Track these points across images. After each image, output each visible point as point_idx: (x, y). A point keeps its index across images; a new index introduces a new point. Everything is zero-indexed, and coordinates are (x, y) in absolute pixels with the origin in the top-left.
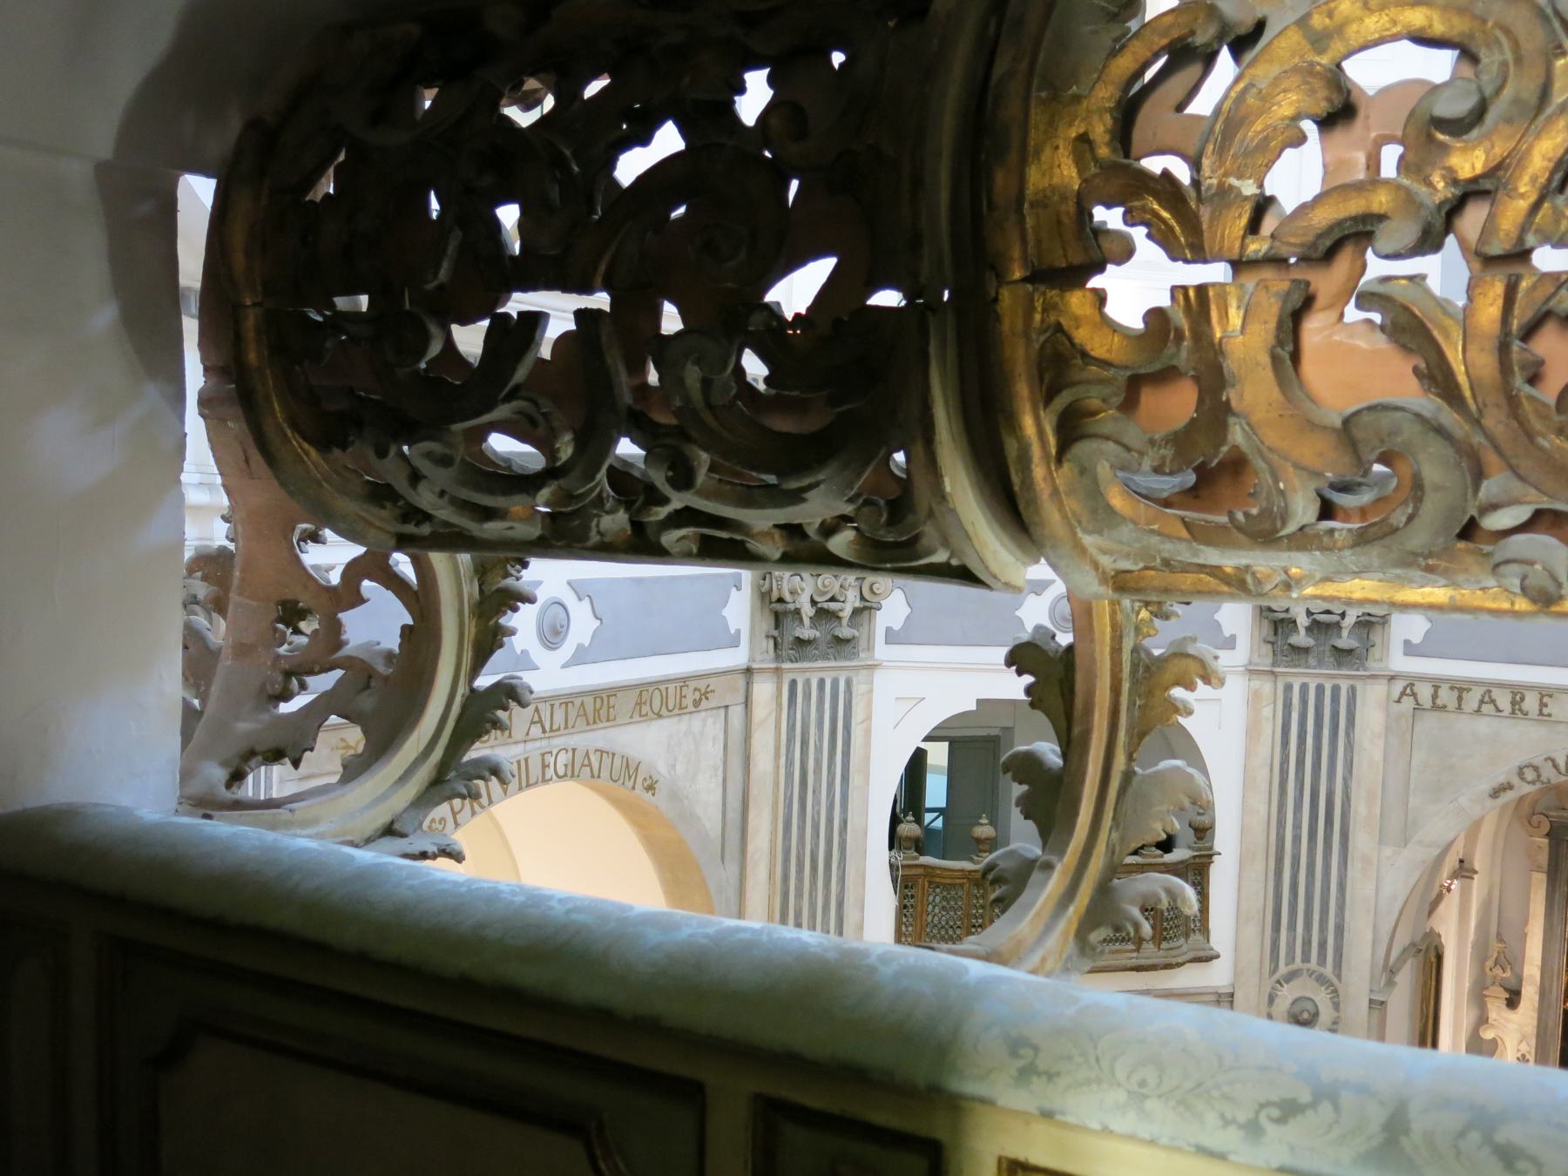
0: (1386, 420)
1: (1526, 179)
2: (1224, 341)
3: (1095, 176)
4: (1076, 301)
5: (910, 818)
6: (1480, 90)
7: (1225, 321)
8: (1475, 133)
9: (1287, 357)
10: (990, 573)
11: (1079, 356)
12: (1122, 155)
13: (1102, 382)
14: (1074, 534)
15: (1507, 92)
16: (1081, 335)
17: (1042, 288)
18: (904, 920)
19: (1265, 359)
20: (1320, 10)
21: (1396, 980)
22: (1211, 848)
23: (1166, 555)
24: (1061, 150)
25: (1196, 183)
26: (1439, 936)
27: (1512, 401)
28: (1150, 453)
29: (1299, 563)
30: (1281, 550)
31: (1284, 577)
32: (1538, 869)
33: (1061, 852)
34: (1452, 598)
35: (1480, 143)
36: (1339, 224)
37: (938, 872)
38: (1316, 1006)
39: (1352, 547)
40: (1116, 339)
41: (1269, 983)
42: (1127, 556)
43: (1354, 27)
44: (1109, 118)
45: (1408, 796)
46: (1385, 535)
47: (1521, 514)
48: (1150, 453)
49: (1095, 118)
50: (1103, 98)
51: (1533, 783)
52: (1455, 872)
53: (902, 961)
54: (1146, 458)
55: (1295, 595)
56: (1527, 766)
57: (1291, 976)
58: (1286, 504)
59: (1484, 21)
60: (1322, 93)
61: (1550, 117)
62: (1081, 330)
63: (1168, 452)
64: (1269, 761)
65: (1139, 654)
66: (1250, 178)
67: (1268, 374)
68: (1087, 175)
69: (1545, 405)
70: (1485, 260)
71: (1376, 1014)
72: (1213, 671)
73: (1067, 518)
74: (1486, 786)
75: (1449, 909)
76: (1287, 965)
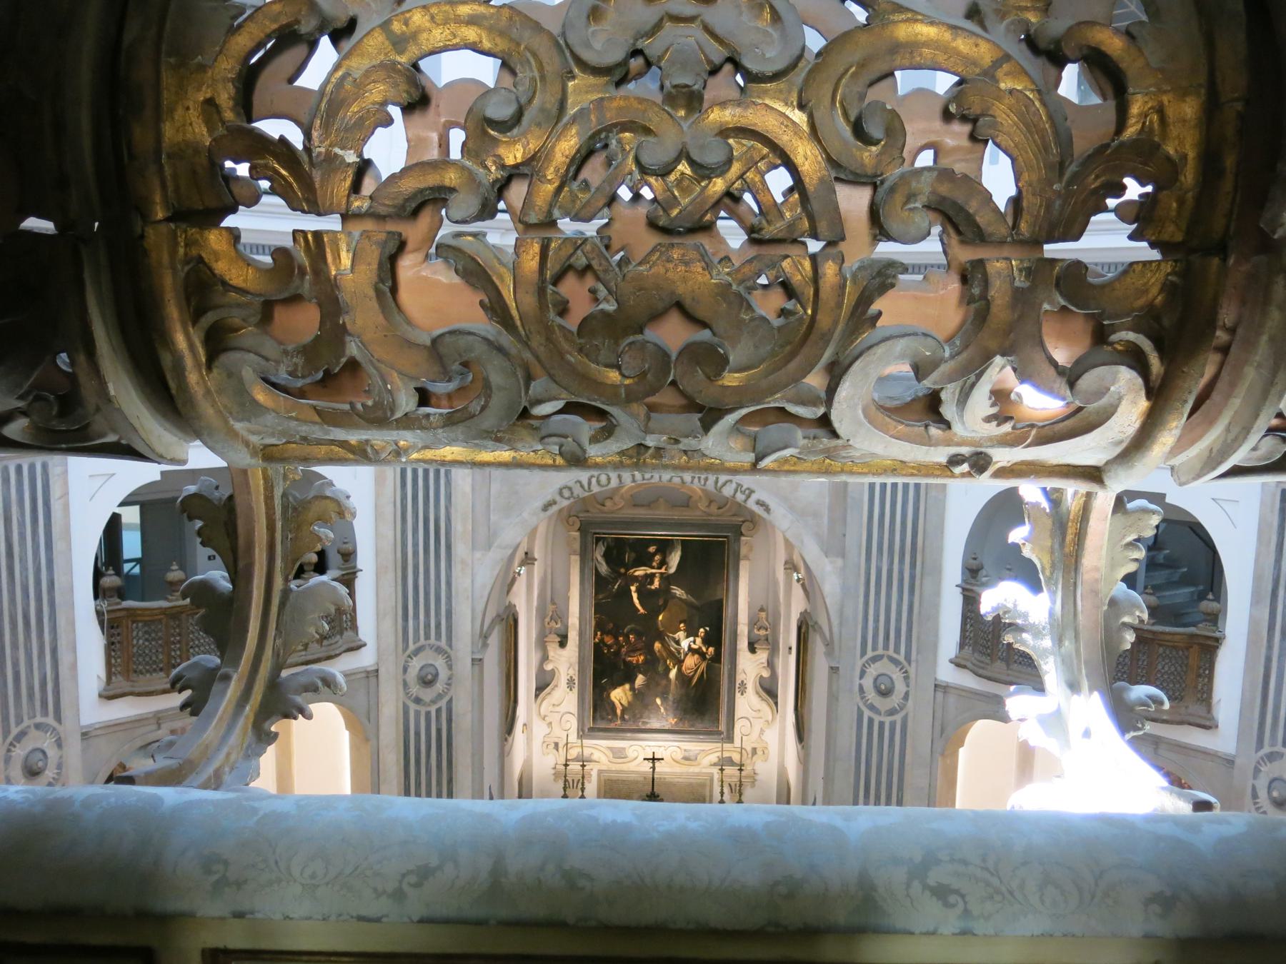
0: (463, 341)
1: (552, 169)
2: (338, 277)
3: (222, 137)
4: (214, 239)
5: (111, 572)
6: (518, 102)
7: (338, 261)
8: (515, 131)
9: (388, 290)
10: (157, 454)
11: (220, 284)
12: (245, 119)
13: (239, 306)
14: (226, 422)
15: (536, 102)
16: (220, 267)
17: (184, 226)
18: (113, 654)
19: (372, 293)
20: (398, 18)
21: (488, 642)
22: (355, 567)
23: (303, 434)
24: (191, 111)
25: (307, 149)
26: (515, 606)
27: (548, 330)
28: (285, 360)
29: (406, 438)
30: (392, 429)
31: (395, 447)
32: (574, 553)
33: (235, 662)
34: (514, 458)
35: (519, 140)
36: (421, 191)
37: (140, 612)
38: (437, 670)
39: (443, 427)
40: (250, 271)
41: (403, 658)
42: (273, 435)
43: (425, 35)
44: (232, 87)
45: (489, 515)
46: (467, 419)
47: (559, 405)
48: (285, 360)
49: (220, 86)
50: (225, 69)
52: (522, 561)
53: (104, 804)
54: (282, 365)
55: (404, 460)
56: (564, 488)
57: (417, 652)
58: (393, 400)
59: (518, 44)
60: (403, 87)
61: (566, 125)
62: (219, 263)
63: (299, 360)
64: (393, 500)
65: (288, 499)
66: (351, 149)
67: (374, 304)
68: (216, 134)
69: (570, 331)
70: (524, 225)
71: (476, 668)
72: (346, 508)
73: (221, 412)
74: (539, 503)
75: (520, 587)
76: (414, 643)
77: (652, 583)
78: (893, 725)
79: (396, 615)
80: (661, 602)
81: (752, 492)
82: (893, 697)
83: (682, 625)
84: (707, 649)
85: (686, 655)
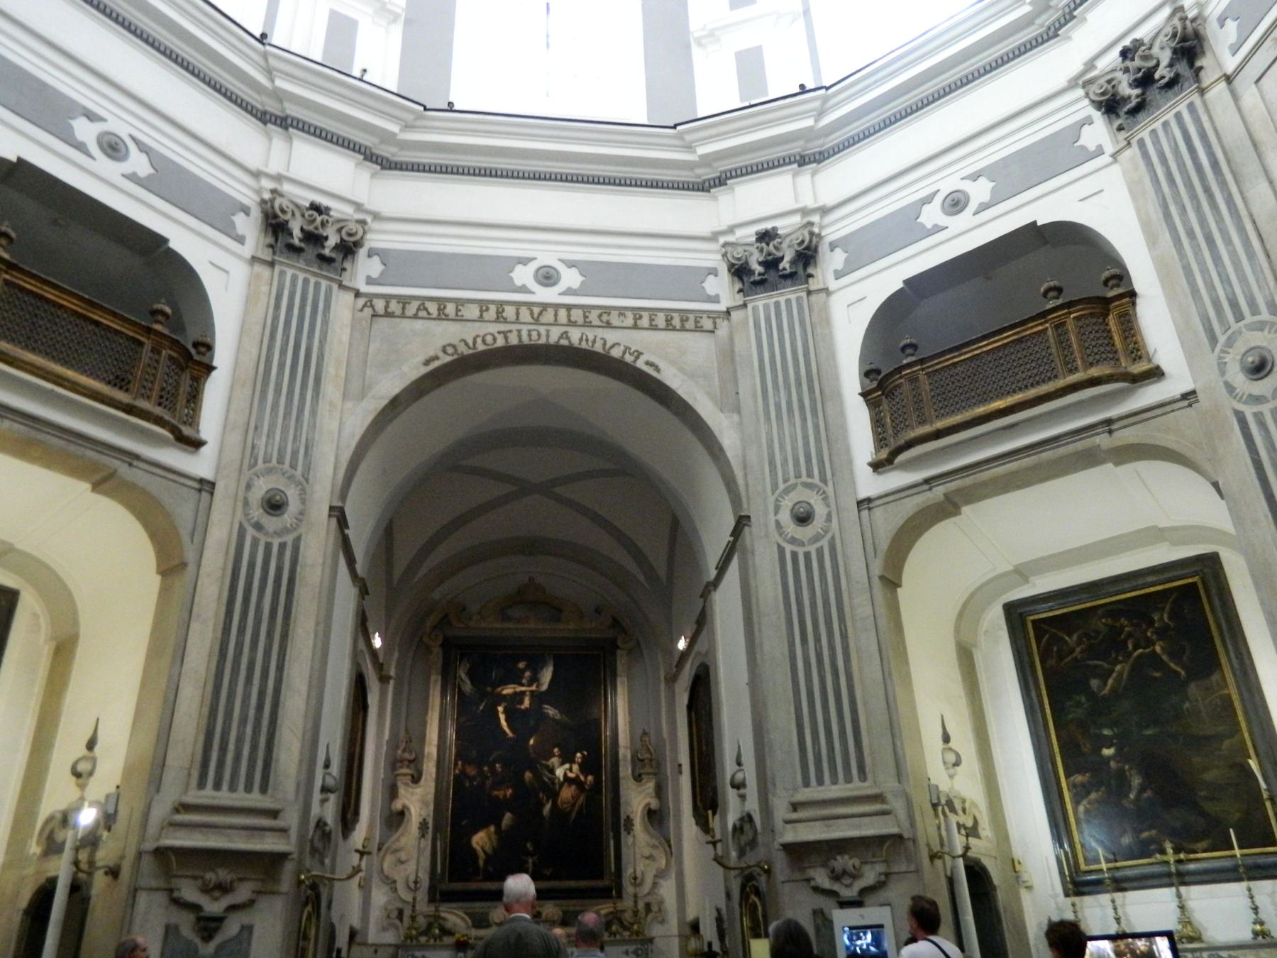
51: (452, 355)
77: (522, 702)
78: (820, 552)
79: (262, 342)
80: (532, 723)
81: (640, 354)
82: (815, 522)
83: (556, 750)
84: (586, 777)
85: (561, 785)
